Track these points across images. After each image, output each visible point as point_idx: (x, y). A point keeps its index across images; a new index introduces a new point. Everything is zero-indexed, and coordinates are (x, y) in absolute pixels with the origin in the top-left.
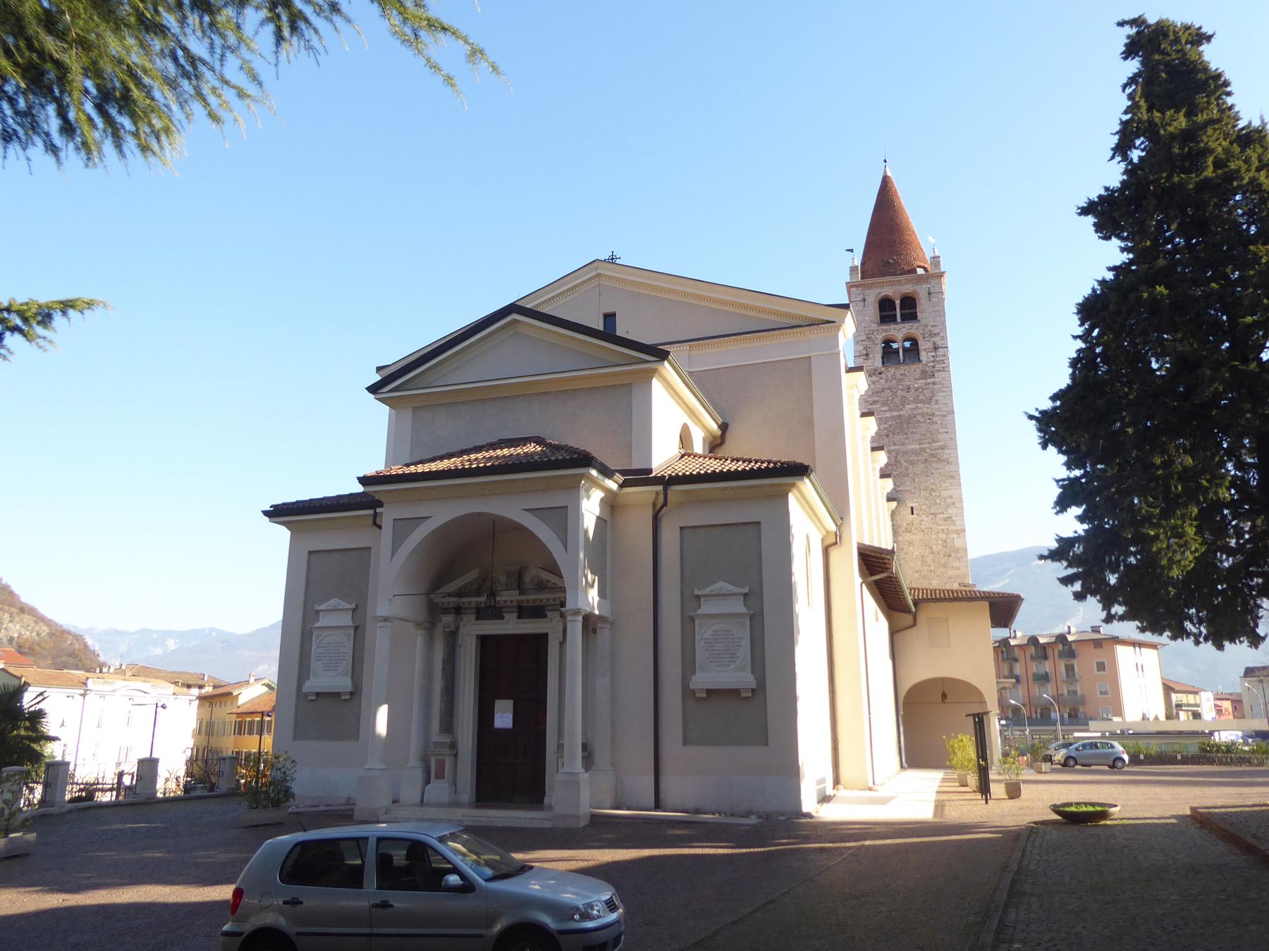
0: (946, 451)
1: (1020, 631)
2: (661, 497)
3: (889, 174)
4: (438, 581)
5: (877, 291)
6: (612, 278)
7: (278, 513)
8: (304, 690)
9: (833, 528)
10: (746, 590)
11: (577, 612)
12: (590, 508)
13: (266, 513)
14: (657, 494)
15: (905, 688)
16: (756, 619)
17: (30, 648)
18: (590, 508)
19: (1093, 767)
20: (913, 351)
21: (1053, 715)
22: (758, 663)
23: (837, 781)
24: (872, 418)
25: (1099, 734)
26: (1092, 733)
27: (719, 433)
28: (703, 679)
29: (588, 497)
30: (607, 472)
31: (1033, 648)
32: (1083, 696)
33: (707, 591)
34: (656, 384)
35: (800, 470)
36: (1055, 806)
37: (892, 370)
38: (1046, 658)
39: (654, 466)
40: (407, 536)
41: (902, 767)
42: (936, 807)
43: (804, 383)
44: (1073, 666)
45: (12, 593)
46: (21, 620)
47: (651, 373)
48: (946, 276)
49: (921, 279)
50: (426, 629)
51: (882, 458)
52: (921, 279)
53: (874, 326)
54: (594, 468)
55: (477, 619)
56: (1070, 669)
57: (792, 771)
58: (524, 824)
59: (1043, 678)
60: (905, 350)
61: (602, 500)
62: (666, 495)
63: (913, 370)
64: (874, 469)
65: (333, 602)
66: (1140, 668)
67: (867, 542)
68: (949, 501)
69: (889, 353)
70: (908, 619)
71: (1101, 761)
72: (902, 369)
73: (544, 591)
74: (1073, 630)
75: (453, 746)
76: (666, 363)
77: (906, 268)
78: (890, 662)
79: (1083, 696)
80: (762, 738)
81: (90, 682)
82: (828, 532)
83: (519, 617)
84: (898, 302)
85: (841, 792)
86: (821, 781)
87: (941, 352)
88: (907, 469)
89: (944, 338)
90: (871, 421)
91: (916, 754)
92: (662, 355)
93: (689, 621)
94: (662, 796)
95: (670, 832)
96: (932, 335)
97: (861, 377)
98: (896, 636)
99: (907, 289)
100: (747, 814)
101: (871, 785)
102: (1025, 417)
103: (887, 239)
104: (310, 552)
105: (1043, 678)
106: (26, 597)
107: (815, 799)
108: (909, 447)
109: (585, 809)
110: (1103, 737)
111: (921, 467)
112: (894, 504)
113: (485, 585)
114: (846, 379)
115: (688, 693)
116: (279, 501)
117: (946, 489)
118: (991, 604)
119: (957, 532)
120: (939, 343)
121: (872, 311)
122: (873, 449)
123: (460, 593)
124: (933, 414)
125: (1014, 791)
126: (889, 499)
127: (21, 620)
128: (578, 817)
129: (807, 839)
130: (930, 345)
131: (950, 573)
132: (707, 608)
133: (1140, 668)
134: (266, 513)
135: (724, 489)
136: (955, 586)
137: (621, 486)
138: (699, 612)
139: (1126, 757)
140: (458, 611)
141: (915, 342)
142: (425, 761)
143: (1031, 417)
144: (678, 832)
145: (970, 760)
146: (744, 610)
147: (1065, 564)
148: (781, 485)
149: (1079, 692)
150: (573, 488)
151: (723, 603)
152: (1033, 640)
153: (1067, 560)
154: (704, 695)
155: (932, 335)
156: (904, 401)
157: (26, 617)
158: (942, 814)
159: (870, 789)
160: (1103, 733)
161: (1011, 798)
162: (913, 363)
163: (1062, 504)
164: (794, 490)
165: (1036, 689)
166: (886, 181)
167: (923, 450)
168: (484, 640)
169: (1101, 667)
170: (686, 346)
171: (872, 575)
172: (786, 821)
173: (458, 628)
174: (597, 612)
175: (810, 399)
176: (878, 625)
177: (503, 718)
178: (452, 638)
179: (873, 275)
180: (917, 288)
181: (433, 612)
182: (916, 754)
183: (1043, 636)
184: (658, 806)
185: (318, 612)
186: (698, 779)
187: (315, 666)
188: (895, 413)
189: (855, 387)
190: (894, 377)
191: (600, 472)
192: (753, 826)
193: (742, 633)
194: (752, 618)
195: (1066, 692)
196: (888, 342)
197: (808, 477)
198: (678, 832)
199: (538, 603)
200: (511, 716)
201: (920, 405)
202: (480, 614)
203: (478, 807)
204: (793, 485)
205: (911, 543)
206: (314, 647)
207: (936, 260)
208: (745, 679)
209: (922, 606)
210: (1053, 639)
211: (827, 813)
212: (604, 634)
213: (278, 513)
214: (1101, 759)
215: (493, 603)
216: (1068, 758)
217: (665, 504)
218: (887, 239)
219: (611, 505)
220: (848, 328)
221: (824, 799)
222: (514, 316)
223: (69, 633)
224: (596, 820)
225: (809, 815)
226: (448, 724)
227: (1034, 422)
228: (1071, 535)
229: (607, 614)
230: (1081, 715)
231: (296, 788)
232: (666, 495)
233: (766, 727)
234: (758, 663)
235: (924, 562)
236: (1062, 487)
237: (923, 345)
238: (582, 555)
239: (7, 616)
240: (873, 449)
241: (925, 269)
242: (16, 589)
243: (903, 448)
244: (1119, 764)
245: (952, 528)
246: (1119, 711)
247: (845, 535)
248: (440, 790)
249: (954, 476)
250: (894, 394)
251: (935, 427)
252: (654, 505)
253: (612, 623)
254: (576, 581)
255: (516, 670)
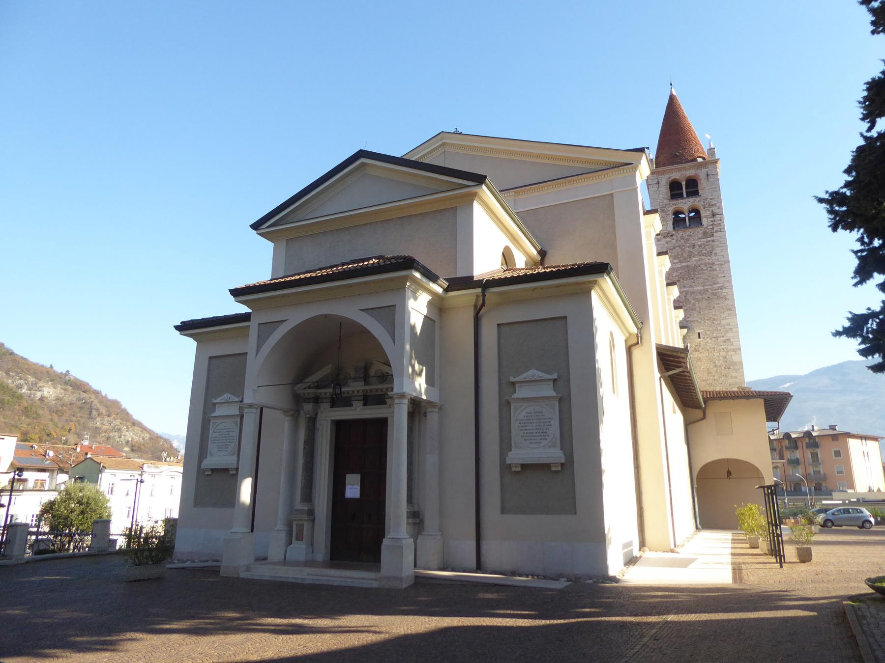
0: (724, 291)
1: (792, 423)
2: (481, 298)
3: (674, 93)
4: (301, 376)
5: (667, 176)
6: (453, 145)
7: (185, 328)
8: (202, 467)
9: (634, 330)
10: (555, 376)
11: (402, 396)
12: (417, 309)
13: (177, 328)
14: (478, 296)
15: (698, 467)
16: (564, 401)
17: (139, 447)
18: (417, 309)
19: (844, 528)
20: (696, 218)
21: (803, 489)
22: (566, 441)
23: (642, 544)
24: (667, 256)
25: (841, 502)
26: (835, 501)
27: (539, 258)
28: (518, 455)
29: (416, 299)
30: (432, 277)
31: (787, 441)
32: (825, 474)
33: (521, 378)
34: (476, 206)
35: (601, 269)
36: (869, 580)
37: (681, 233)
38: (797, 448)
39: (475, 274)
40: (268, 336)
41: (697, 528)
42: (734, 569)
43: (607, 212)
44: (817, 454)
45: (128, 414)
46: (133, 430)
47: (472, 196)
48: (719, 162)
49: (700, 165)
50: (292, 416)
51: (675, 292)
52: (700, 165)
53: (666, 202)
54: (417, 270)
55: (332, 407)
56: (815, 456)
57: (597, 538)
58: (356, 584)
59: (795, 462)
60: (690, 218)
61: (429, 302)
62: (484, 296)
63: (699, 231)
64: (669, 299)
65: (226, 396)
66: (866, 454)
67: (664, 343)
68: (727, 327)
69: (678, 221)
70: (698, 413)
71: (853, 523)
72: (689, 232)
73: (378, 380)
74: (816, 428)
75: (311, 513)
76: (484, 186)
77: (690, 158)
78: (686, 447)
79: (825, 474)
80: (572, 509)
81: (145, 467)
82: (630, 334)
83: (365, 404)
84: (684, 183)
85: (647, 554)
86: (629, 544)
87: (718, 217)
88: (694, 305)
89: (720, 207)
90: (666, 258)
91: (709, 517)
92: (480, 179)
93: (505, 405)
94: (483, 559)
95: (481, 596)
96: (711, 205)
97: (656, 218)
98: (690, 427)
99: (691, 173)
100: (556, 579)
101: (672, 547)
102: (815, 201)
103: (674, 134)
104: (210, 358)
105: (795, 462)
106: (136, 416)
107: (621, 561)
108: (696, 288)
109: (408, 570)
110: (844, 504)
111: (704, 303)
112: (685, 330)
113: (337, 380)
114: (644, 220)
115: (505, 468)
116: (188, 318)
117: (725, 318)
118: (765, 400)
119: (734, 350)
120: (716, 211)
121: (665, 190)
122: (668, 285)
123: (319, 385)
124: (713, 264)
125: (805, 556)
126: (682, 327)
127: (133, 430)
128: (401, 579)
129: (609, 609)
130: (709, 213)
131: (730, 381)
132: (521, 393)
133: (866, 454)
134: (177, 328)
135: (534, 289)
136: (736, 389)
137: (446, 290)
138: (515, 396)
139: (872, 520)
140: (317, 400)
141: (697, 212)
142: (289, 525)
143: (821, 200)
144: (488, 596)
145: (761, 527)
146: (553, 394)
147: (860, 340)
148: (584, 283)
149: (822, 472)
150: (399, 288)
151: (535, 388)
152: (787, 436)
153: (861, 336)
154: (519, 469)
155: (711, 205)
156: (690, 255)
157: (136, 428)
158: (741, 578)
159: (672, 551)
160: (844, 501)
161: (803, 561)
162: (697, 226)
163: (863, 273)
164: (596, 288)
165: (790, 470)
166: (672, 100)
167: (707, 290)
168: (339, 425)
169: (837, 454)
170: (512, 193)
171: (668, 370)
172: (590, 588)
173: (316, 414)
174: (424, 397)
175: (613, 228)
176: (675, 418)
177: (353, 490)
178: (312, 421)
179: (664, 165)
180: (698, 172)
181: (298, 400)
182: (709, 517)
183: (795, 432)
184: (479, 568)
185: (215, 404)
186: (514, 546)
187: (212, 447)
188: (685, 264)
189: (652, 226)
190: (682, 238)
191: (423, 274)
192: (559, 591)
193: (553, 414)
194: (560, 400)
195: (812, 472)
196: (677, 213)
197: (608, 274)
198: (488, 596)
199: (380, 393)
200: (359, 487)
201: (703, 257)
202: (338, 401)
203: (332, 566)
204: (595, 282)
205: (699, 360)
206: (211, 432)
207: (712, 151)
208: (553, 454)
209: (710, 402)
210: (802, 435)
211: (635, 577)
212: (433, 418)
213: (185, 328)
214: (851, 522)
215: (338, 391)
216: (826, 521)
217: (483, 305)
218: (674, 134)
219: (438, 307)
220: (644, 170)
221: (631, 561)
222: (363, 160)
223: (161, 438)
224: (422, 582)
225: (614, 579)
226: (308, 495)
227: (824, 205)
228: (865, 312)
229: (435, 399)
230: (823, 488)
231: (177, 549)
232: (484, 296)
233: (574, 498)
234: (566, 441)
235: (709, 373)
236: (859, 258)
237: (703, 213)
238: (408, 347)
239: (125, 427)
240: (668, 285)
241: (704, 159)
242: (130, 411)
243: (691, 289)
244: (868, 525)
245: (730, 347)
246: (852, 486)
247: (645, 336)
248: (299, 550)
249: (731, 309)
250: (683, 250)
251: (715, 272)
252: (475, 306)
253: (440, 408)
254: (402, 370)
255: (361, 448)
